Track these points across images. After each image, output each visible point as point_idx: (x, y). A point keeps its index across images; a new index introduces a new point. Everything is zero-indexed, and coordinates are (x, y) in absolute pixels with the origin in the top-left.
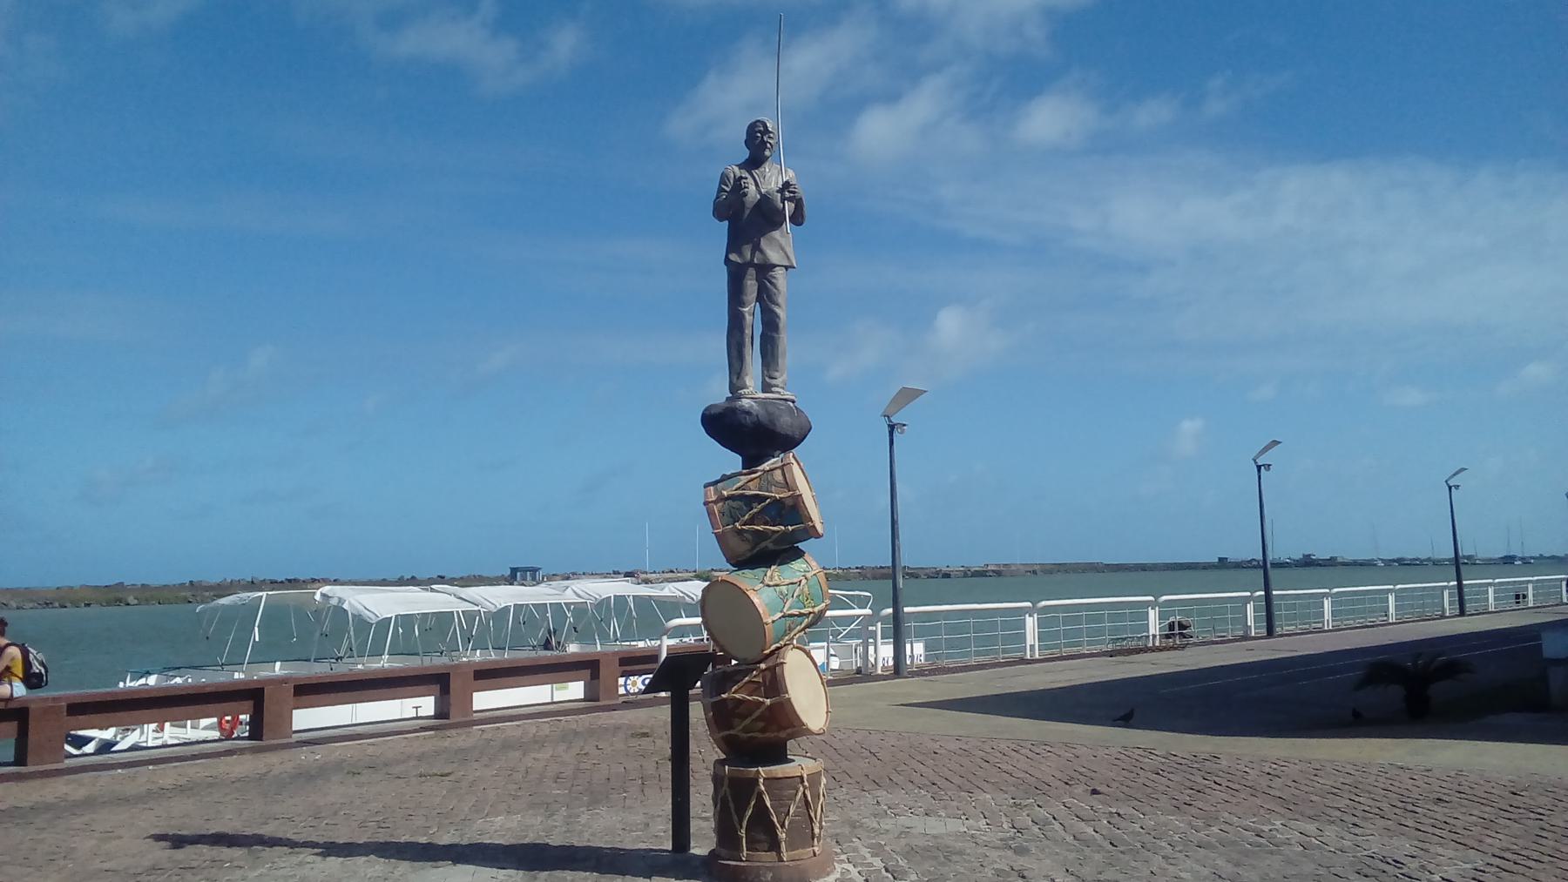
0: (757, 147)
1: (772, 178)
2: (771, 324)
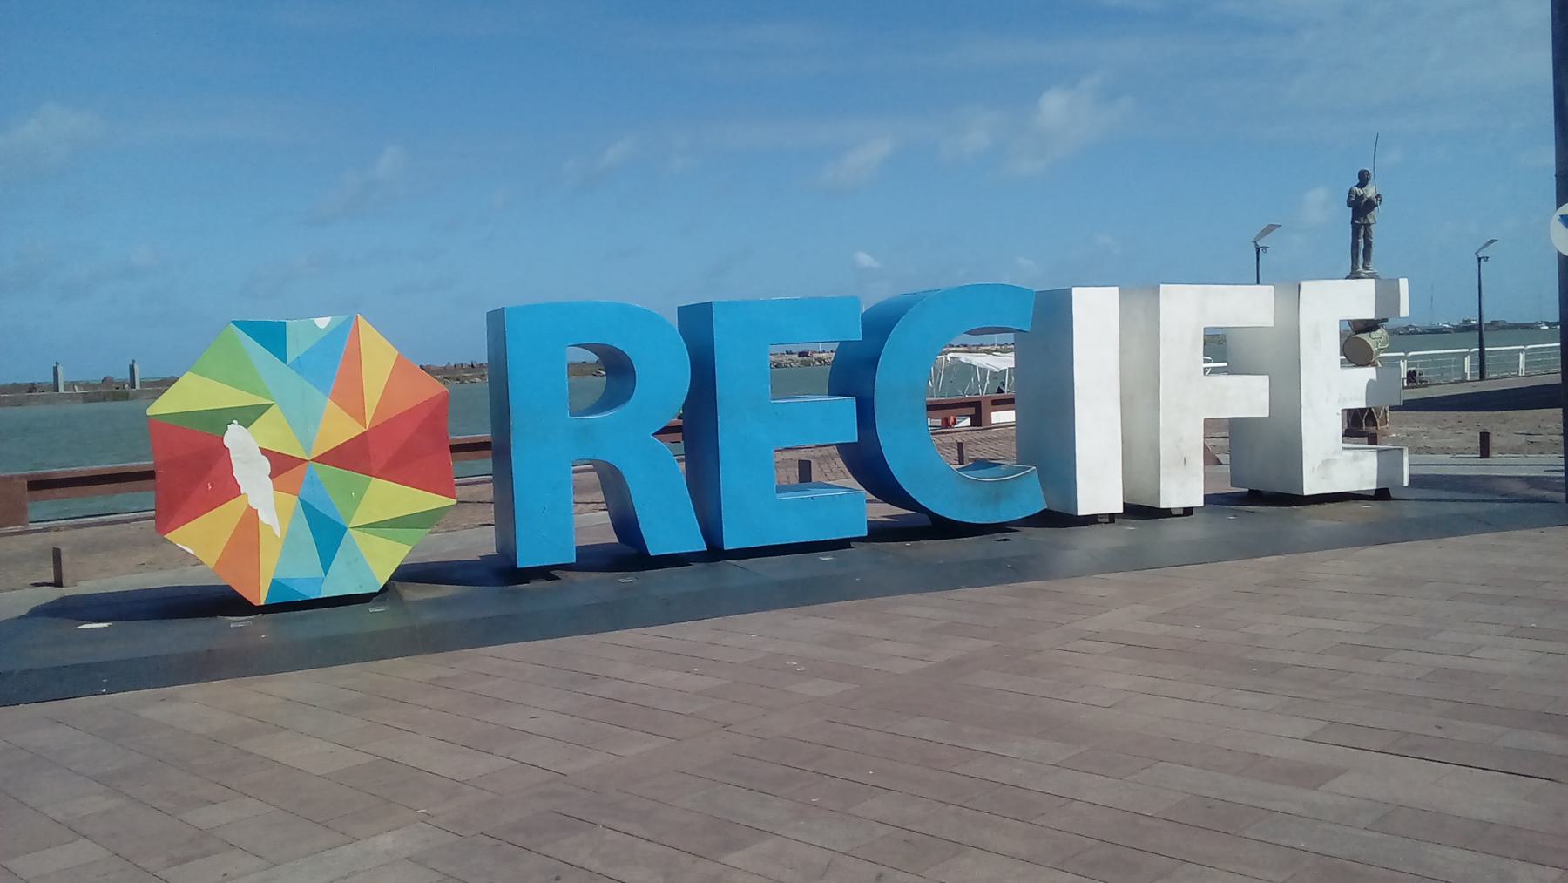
1: (1370, 191)
2: (1368, 245)
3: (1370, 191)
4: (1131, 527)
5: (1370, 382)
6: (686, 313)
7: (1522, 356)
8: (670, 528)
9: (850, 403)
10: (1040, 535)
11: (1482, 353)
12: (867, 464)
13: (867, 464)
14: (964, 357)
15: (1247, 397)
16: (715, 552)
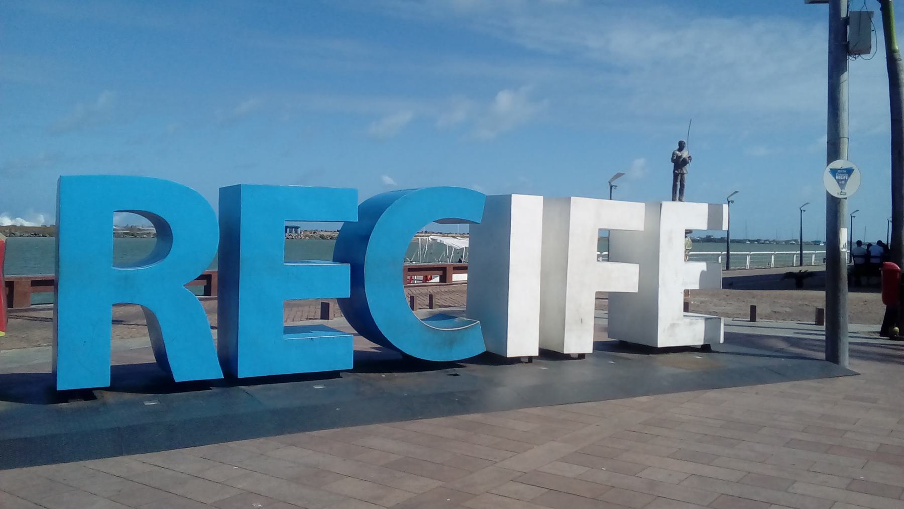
0: (681, 146)
2: (682, 186)
3: (685, 154)
4: (545, 367)
5: (703, 273)
6: (224, 192)
7: (748, 258)
8: (194, 361)
9: (346, 268)
10: (479, 370)
11: (728, 255)
12: (358, 315)
13: (358, 315)
14: (439, 239)
15: (624, 278)
16: (231, 379)
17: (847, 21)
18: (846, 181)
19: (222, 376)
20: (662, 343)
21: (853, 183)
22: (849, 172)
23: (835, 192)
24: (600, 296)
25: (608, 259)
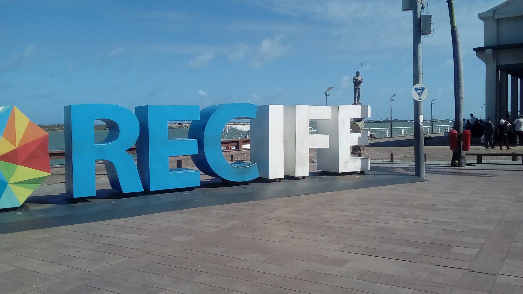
2: (359, 95)
3: (360, 78)
7: (403, 130)
8: (131, 183)
11: (391, 129)
12: (201, 162)
13: (201, 162)
14: (234, 126)
15: (322, 141)
16: (147, 192)
17: (420, 19)
18: (422, 93)
19: (143, 190)
20: (341, 171)
21: (425, 95)
22: (423, 89)
23: (417, 98)
24: (311, 150)
25: (317, 133)
